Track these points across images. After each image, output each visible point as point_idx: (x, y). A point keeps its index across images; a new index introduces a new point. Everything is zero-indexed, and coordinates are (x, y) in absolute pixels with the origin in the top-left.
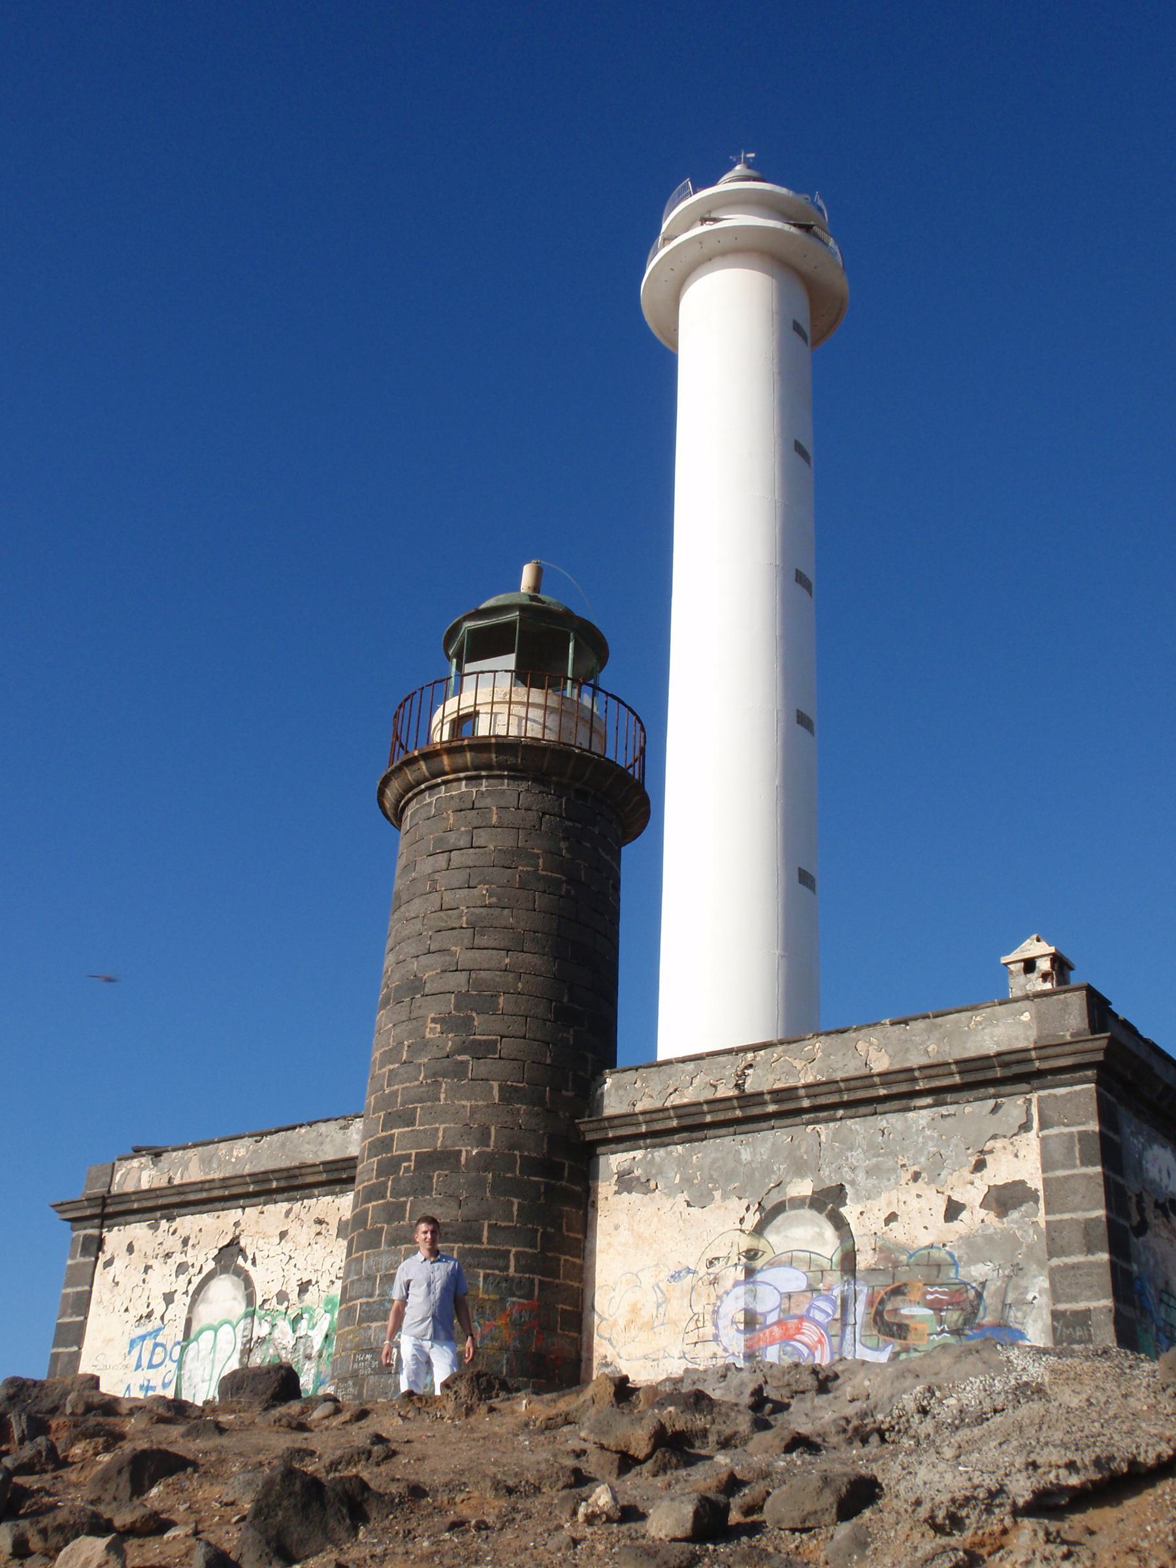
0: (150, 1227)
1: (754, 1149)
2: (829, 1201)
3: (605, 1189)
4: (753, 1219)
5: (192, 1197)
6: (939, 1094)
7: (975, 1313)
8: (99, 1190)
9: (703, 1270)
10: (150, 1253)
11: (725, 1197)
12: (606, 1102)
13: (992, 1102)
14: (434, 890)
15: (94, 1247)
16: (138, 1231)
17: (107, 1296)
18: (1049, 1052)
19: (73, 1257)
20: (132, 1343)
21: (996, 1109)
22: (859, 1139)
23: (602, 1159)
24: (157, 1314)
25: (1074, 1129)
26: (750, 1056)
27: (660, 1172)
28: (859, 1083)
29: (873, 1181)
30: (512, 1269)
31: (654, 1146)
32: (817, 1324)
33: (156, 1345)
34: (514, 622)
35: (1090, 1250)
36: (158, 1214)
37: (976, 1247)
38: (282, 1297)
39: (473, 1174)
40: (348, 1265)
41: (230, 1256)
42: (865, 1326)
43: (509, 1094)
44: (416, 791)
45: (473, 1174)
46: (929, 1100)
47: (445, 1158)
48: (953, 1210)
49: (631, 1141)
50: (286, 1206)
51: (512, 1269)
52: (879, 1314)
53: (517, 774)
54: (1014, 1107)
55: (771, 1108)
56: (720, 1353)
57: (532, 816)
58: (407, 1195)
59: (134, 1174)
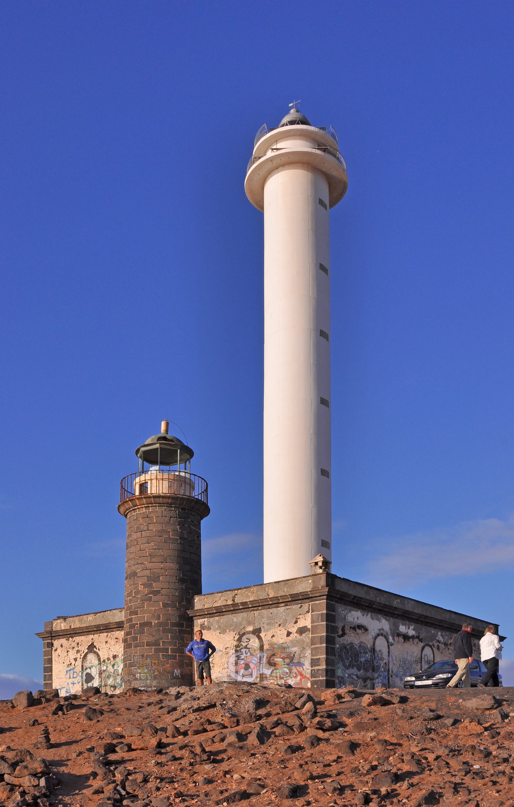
0: (66, 640)
2: (257, 632)
4: (237, 637)
5: (78, 632)
6: (286, 603)
7: (293, 660)
8: (49, 629)
9: (224, 651)
10: (68, 647)
11: (229, 631)
12: (195, 605)
13: (300, 605)
14: (137, 544)
15: (51, 646)
16: (63, 641)
17: (57, 659)
18: (313, 592)
19: (45, 648)
20: (67, 672)
21: (301, 607)
22: (265, 615)
23: (195, 621)
24: (73, 664)
25: (320, 612)
26: (236, 591)
27: (212, 625)
28: (264, 601)
29: (268, 627)
30: (170, 653)
31: (210, 617)
32: (253, 663)
33: (74, 672)
34: (158, 448)
35: (321, 644)
36: (68, 636)
37: (294, 643)
38: (108, 659)
39: (156, 628)
40: (124, 652)
41: (92, 648)
42: (266, 664)
43: (165, 605)
44: (129, 510)
45: (156, 628)
46: (283, 605)
47: (148, 624)
48: (289, 634)
50: (106, 634)
51: (170, 653)
52: (269, 660)
53: (161, 505)
54: (306, 606)
55: (241, 607)
56: (229, 671)
57: (167, 519)
58: (138, 634)
59: (59, 624)
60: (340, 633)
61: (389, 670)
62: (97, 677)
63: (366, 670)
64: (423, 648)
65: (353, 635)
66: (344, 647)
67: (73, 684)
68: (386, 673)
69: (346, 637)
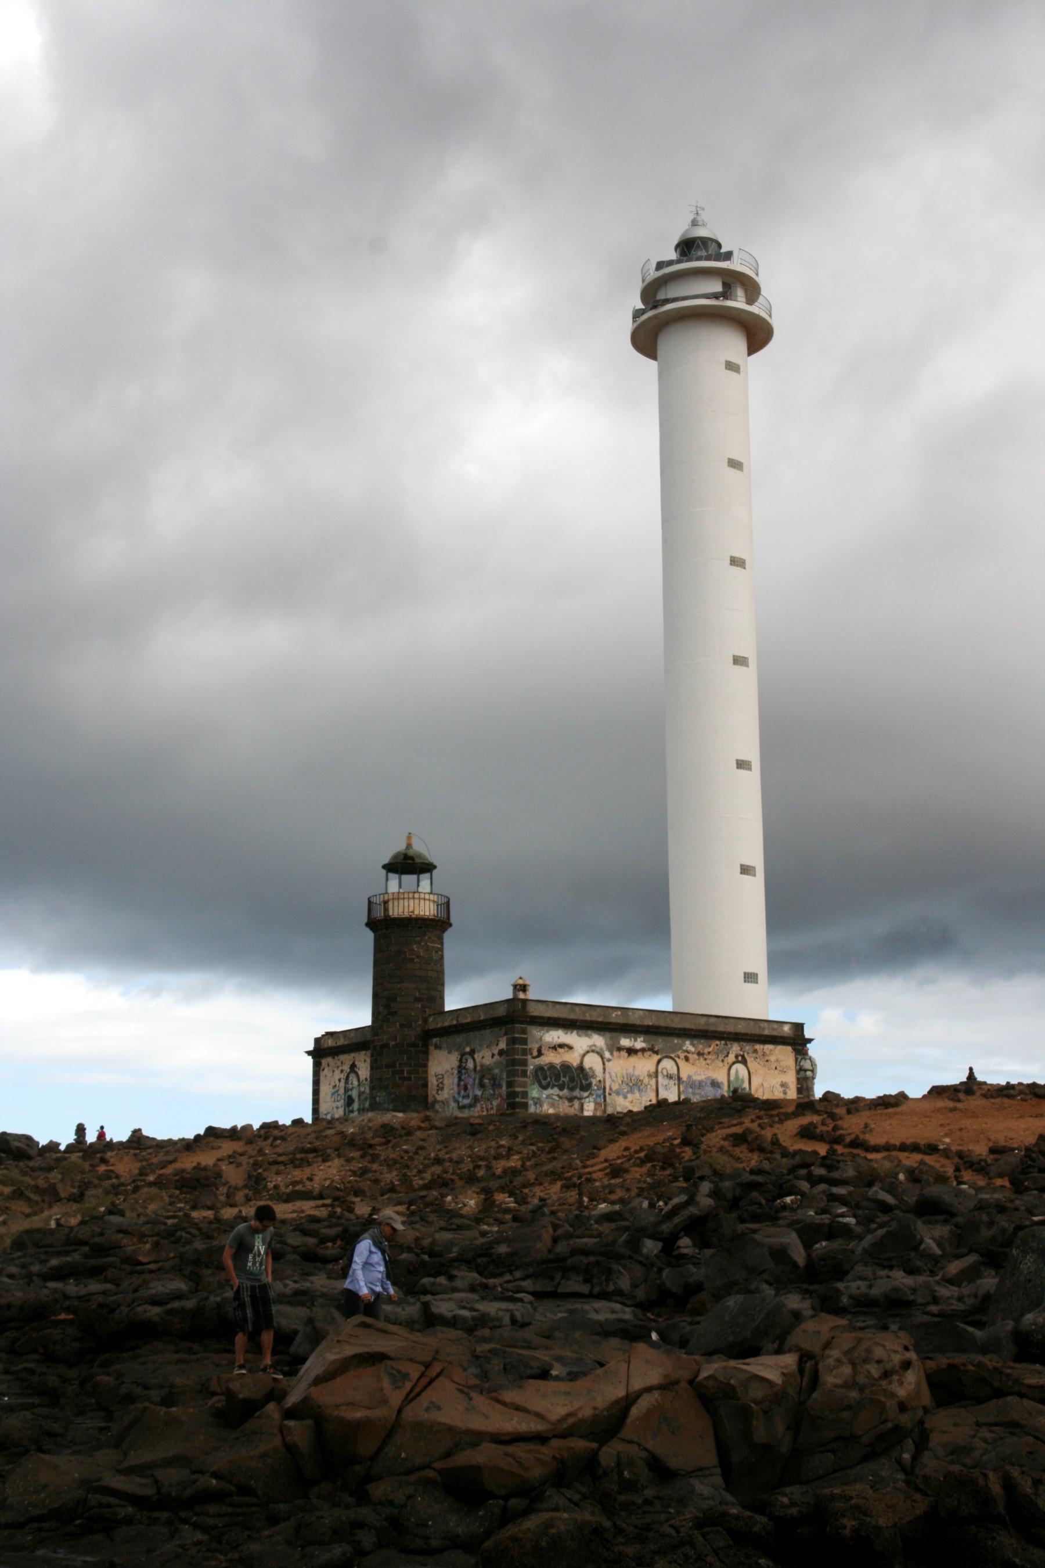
1: (459, 1039)
3: (432, 1048)
16: (329, 1059)
48: (493, 1055)
49: (435, 1036)
60: (535, 1053)
61: (605, 1088)
62: (356, 1100)
63: (571, 1089)
64: (659, 1062)
65: (552, 1055)
66: (540, 1069)
67: (337, 1108)
68: (601, 1092)
69: (542, 1058)
